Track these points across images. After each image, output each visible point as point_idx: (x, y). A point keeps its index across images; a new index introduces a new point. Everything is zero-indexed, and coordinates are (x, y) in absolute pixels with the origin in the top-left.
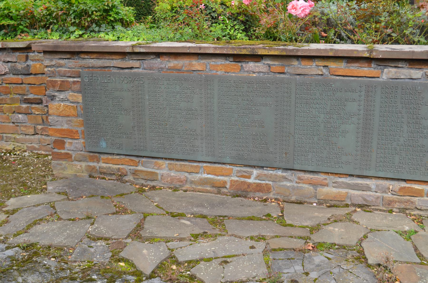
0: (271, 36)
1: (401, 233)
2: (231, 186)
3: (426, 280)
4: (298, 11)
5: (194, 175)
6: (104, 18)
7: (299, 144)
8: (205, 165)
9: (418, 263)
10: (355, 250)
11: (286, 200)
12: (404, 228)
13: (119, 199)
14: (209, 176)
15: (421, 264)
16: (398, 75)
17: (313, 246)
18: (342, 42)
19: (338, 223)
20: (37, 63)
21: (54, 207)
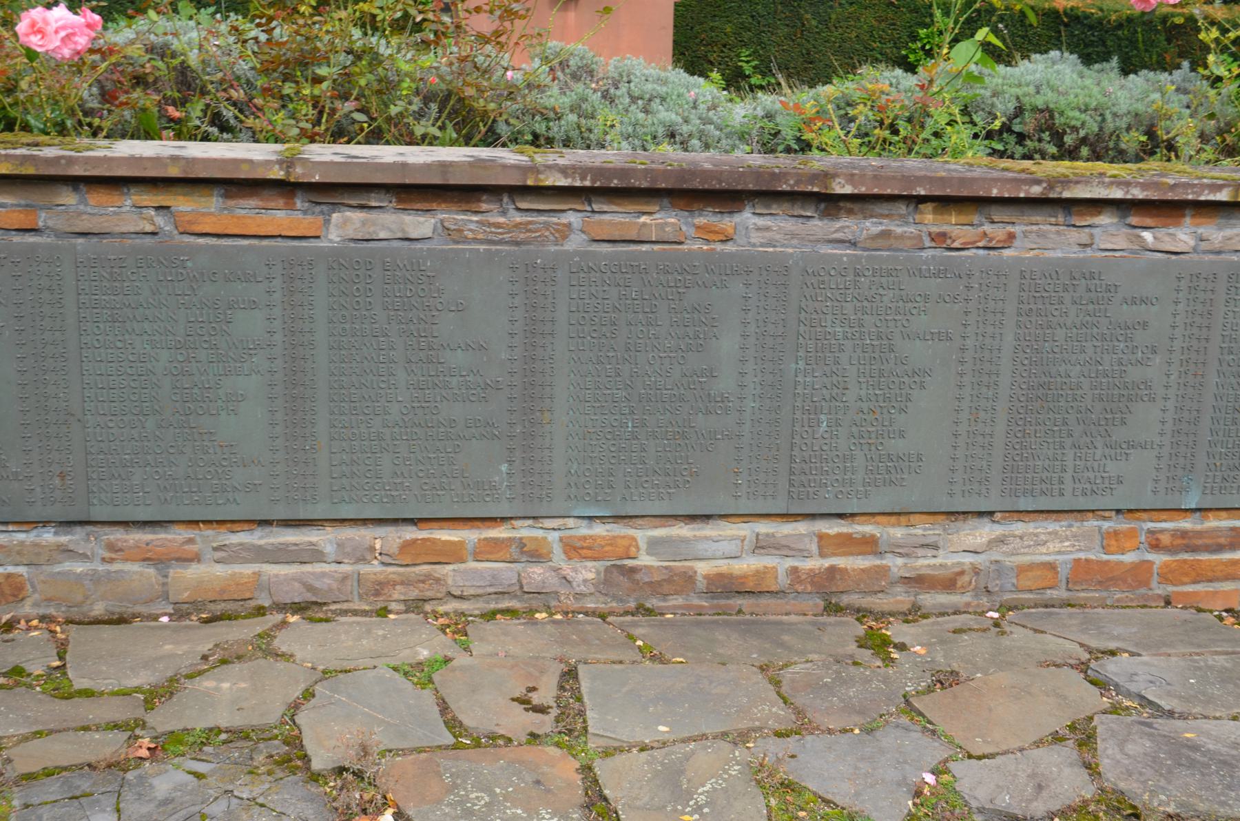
1: (407, 668)
3: (465, 789)
4: (51, 42)
7: (102, 444)
9: (447, 747)
10: (276, 737)
11: (77, 618)
12: (417, 653)
15: (455, 747)
16: (371, 230)
17: (153, 746)
18: (225, 135)
19: (231, 666)
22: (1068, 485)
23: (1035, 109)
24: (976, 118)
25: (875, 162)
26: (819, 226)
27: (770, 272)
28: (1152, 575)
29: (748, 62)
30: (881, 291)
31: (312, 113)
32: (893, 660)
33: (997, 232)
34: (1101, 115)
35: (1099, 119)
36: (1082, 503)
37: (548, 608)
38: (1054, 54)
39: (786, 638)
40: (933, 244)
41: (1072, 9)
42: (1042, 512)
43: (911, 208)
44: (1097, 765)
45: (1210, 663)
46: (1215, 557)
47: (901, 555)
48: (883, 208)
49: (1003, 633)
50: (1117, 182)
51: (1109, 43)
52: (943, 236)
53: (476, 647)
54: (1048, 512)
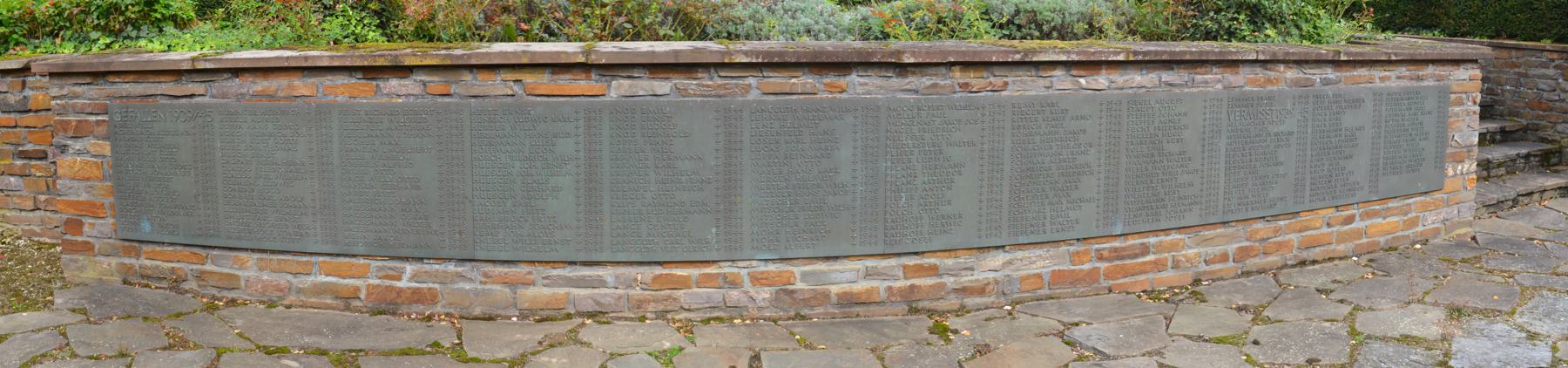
0: (424, 34)
2: (368, 295)
5: (303, 278)
6: (146, 16)
8: (321, 259)
13: (173, 323)
14: (330, 279)
20: (40, 92)
21: (64, 335)
22: (1048, 227)
25: (927, 44)
26: (896, 81)
27: (868, 109)
31: (601, 24)
33: (998, 81)
37: (742, 317)
52: (967, 84)
53: (698, 341)
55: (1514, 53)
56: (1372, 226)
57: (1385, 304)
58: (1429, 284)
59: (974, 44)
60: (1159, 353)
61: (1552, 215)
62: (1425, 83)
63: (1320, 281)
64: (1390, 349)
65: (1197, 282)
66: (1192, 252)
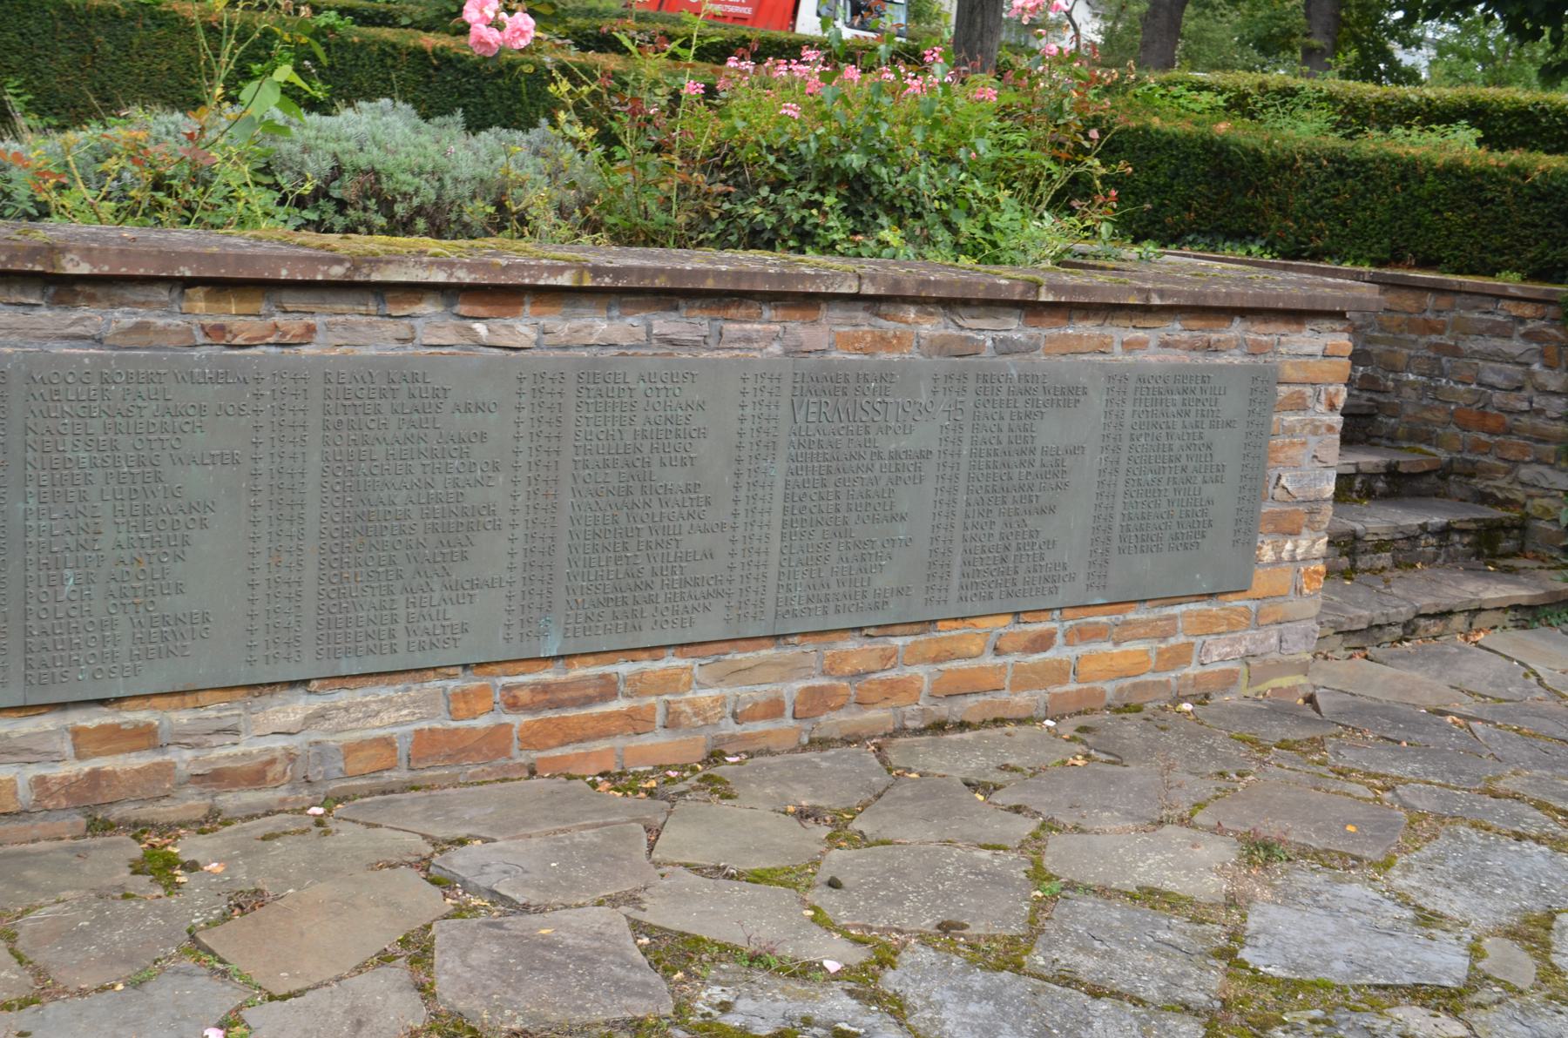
22: (401, 640)
23: (357, 170)
24: (282, 180)
26: (47, 317)
28: (511, 741)
29: (17, 95)
30: (140, 403)
32: (178, 885)
33: (292, 324)
34: (439, 179)
35: (437, 184)
36: (419, 660)
38: (385, 102)
39: (30, 873)
40: (208, 341)
41: (442, 49)
42: (371, 675)
43: (176, 293)
44: (432, 984)
45: (577, 839)
46: (583, 712)
47: (190, 746)
48: (138, 294)
49: (326, 833)
50: (439, 262)
51: (488, 93)
52: (220, 330)
54: (379, 674)
55: (1430, 300)
56: (1089, 658)
57: (1108, 820)
58: (1207, 788)
59: (237, 240)
60: (633, 900)
61: (1498, 662)
62: (1223, 359)
63: (975, 764)
64: (1115, 914)
65: (715, 756)
66: (705, 695)
